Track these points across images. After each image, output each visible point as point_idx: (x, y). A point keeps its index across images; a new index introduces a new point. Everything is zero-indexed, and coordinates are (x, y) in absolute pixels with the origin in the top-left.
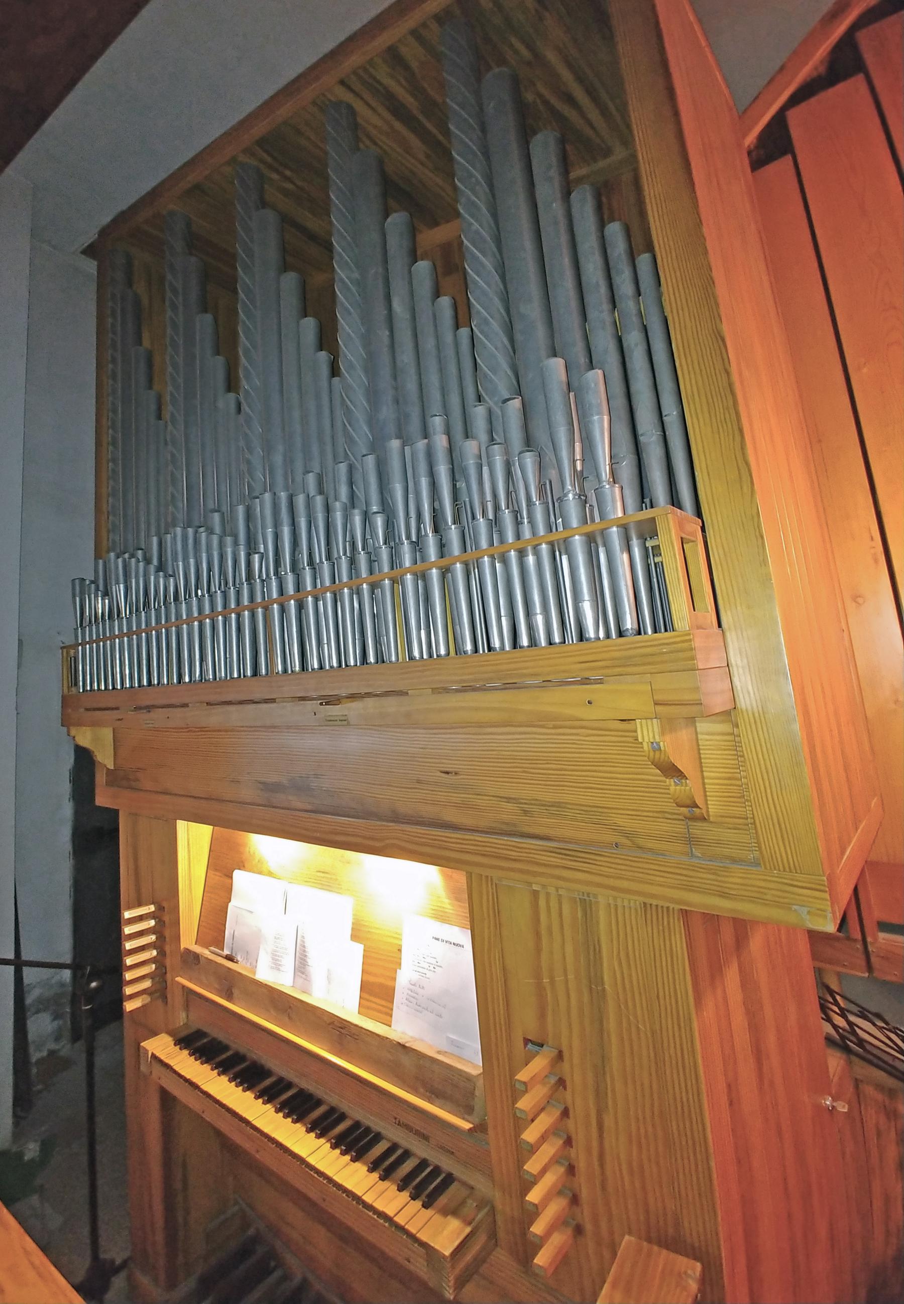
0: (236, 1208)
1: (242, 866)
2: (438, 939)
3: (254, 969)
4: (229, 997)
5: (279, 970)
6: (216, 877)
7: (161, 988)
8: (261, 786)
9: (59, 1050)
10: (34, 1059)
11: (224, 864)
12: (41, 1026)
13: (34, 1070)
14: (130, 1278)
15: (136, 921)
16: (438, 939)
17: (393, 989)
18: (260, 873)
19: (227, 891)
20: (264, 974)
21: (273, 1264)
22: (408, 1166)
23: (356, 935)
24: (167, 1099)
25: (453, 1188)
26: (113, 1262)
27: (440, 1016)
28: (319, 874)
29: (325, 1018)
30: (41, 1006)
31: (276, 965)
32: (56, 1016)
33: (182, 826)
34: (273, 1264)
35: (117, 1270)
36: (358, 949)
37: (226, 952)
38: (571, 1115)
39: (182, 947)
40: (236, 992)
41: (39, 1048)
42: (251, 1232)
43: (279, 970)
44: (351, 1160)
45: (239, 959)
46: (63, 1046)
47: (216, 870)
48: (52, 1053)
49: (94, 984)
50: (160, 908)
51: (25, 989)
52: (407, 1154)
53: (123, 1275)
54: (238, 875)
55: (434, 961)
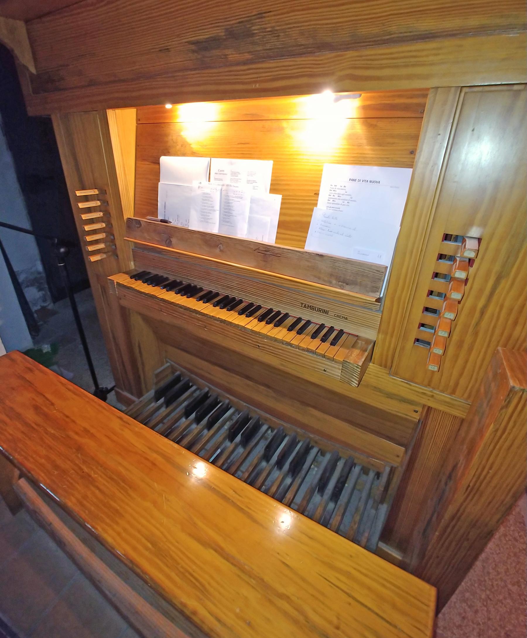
0: (168, 364)
1: (167, 153)
2: (354, 180)
3: (188, 221)
4: (169, 244)
5: (207, 222)
6: (146, 166)
7: (112, 251)
8: (193, 47)
9: (46, 306)
10: (33, 311)
11: (154, 143)
12: (32, 294)
13: (35, 315)
14: (117, 393)
15: (84, 202)
16: (354, 180)
17: (309, 223)
18: (184, 155)
19: (156, 174)
20: (195, 226)
21: (191, 384)
22: (312, 328)
23: (274, 189)
24: (124, 312)
25: (344, 336)
26: (106, 388)
27: (350, 236)
28: (240, 146)
29: (252, 247)
30: (29, 284)
31: (205, 218)
32: (40, 289)
33: (110, 113)
34: (191, 384)
35: (109, 391)
36: (278, 198)
37: (160, 217)
38: (469, 284)
39: (125, 218)
40: (174, 240)
41: (35, 305)
42: (178, 373)
43: (207, 222)
44: (274, 326)
45: (171, 221)
46: (49, 305)
47: (144, 160)
48: (43, 308)
49: (62, 250)
50: (103, 192)
51: (16, 274)
52: (308, 323)
53: (113, 392)
54: (163, 159)
55: (348, 198)
